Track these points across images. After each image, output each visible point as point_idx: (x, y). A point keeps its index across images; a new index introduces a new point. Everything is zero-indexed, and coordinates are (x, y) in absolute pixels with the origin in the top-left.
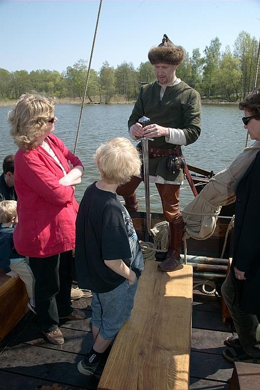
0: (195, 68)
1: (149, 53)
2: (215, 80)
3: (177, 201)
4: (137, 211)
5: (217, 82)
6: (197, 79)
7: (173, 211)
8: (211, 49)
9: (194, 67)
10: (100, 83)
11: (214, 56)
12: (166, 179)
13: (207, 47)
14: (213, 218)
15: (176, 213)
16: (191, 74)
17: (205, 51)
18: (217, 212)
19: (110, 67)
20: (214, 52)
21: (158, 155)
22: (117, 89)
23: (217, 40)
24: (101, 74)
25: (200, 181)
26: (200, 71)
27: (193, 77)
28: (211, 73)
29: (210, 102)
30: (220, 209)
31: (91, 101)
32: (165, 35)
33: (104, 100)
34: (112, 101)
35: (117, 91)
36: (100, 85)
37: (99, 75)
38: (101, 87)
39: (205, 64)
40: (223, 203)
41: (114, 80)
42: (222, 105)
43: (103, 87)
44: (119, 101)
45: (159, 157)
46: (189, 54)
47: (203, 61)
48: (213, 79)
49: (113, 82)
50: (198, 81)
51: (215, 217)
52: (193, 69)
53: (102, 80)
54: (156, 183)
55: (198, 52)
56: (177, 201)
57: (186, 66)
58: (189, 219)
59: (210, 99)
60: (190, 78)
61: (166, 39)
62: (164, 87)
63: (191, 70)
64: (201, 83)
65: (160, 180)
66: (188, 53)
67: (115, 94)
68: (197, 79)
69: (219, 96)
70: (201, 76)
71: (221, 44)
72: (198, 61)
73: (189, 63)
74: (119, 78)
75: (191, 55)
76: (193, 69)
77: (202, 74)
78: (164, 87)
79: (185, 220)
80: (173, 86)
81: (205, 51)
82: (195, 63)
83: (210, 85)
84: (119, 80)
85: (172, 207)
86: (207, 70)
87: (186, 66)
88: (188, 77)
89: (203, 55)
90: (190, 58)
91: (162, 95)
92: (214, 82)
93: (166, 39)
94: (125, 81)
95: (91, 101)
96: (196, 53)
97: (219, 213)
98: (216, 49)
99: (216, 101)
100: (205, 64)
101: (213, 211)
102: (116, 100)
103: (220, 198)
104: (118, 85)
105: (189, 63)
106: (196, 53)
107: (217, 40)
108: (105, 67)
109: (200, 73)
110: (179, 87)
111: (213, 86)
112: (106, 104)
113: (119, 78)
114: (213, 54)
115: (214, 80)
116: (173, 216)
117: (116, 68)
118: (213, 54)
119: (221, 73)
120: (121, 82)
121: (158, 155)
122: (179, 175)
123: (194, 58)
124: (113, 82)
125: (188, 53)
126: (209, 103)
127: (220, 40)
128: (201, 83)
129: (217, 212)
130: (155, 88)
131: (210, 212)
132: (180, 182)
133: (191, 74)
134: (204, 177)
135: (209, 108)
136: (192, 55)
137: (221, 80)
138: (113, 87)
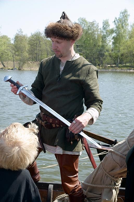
0: (105, 38)
1: (46, 30)
2: (124, 49)
3: (76, 172)
4: (39, 182)
5: (126, 51)
6: (107, 48)
7: (71, 182)
8: (120, 20)
9: (104, 37)
10: (13, 49)
11: (123, 27)
12: (65, 149)
13: (116, 18)
14: (114, 191)
15: (75, 185)
16: (100, 44)
17: (115, 22)
18: (117, 184)
19: (24, 34)
20: (123, 23)
21: (57, 126)
22: (31, 56)
23: (126, 11)
24: (15, 41)
25: (104, 150)
26: (110, 41)
27: (103, 46)
28: (120, 43)
29: (119, 70)
30: (120, 182)
31: (4, 66)
32: (63, 12)
33: (17, 66)
34: (25, 68)
35: (29, 58)
36: (13, 52)
37: (12, 42)
38: (15, 53)
39: (114, 35)
40: (123, 175)
41: (27, 47)
42: (130, 73)
43: (17, 53)
44: (32, 67)
45: (58, 127)
46: (99, 25)
47: (112, 31)
48: (121, 48)
49: (27, 49)
50: (107, 51)
51: (116, 190)
52: (103, 39)
53: (16, 47)
54: (56, 155)
55: (108, 23)
56: (76, 172)
57: (96, 36)
58: (90, 191)
59: (119, 67)
60: (100, 47)
61: (64, 16)
62: (64, 61)
63: (101, 40)
64: (110, 52)
65: (58, 151)
66: (98, 24)
67: (28, 60)
68: (107, 48)
69: (128, 64)
70: (110, 46)
71: (129, 15)
72: (108, 31)
73: (99, 33)
74: (32, 45)
75: (101, 26)
76: (103, 39)
77: (111, 43)
78: (64, 61)
79: (85, 192)
80: (73, 61)
81: (115, 22)
82: (105, 33)
83: (119, 54)
84: (33, 48)
85: (70, 179)
86: (116, 40)
87: (96, 36)
88: (98, 46)
89: (112, 26)
90: (100, 29)
91: (62, 68)
92: (122, 51)
93: (64, 16)
94: (38, 48)
95: (4, 66)
96: (106, 24)
97: (120, 185)
98: (124, 20)
99: (125, 70)
100: (114, 35)
101: (113, 183)
102: (29, 66)
103: (118, 171)
104: (31, 52)
105: (99, 33)
106: (106, 24)
107: (126, 11)
108: (18, 35)
109: (110, 42)
110: (79, 61)
111: (122, 55)
112: (19, 69)
113: (32, 45)
114: (122, 25)
115: (123, 50)
116: (73, 188)
117: (29, 35)
118: (122, 25)
119: (129, 43)
120: (35, 49)
121: (57, 126)
122: (77, 145)
123: (104, 28)
124: (27, 49)
125: (98, 24)
126: (119, 71)
127: (99, 24)
128: (110, 52)
129: (117, 184)
130: (55, 62)
131: (110, 185)
132: (79, 152)
133: (100, 44)
134: (108, 146)
135: (118, 76)
136: (102, 26)
137: (130, 49)
138: (26, 54)
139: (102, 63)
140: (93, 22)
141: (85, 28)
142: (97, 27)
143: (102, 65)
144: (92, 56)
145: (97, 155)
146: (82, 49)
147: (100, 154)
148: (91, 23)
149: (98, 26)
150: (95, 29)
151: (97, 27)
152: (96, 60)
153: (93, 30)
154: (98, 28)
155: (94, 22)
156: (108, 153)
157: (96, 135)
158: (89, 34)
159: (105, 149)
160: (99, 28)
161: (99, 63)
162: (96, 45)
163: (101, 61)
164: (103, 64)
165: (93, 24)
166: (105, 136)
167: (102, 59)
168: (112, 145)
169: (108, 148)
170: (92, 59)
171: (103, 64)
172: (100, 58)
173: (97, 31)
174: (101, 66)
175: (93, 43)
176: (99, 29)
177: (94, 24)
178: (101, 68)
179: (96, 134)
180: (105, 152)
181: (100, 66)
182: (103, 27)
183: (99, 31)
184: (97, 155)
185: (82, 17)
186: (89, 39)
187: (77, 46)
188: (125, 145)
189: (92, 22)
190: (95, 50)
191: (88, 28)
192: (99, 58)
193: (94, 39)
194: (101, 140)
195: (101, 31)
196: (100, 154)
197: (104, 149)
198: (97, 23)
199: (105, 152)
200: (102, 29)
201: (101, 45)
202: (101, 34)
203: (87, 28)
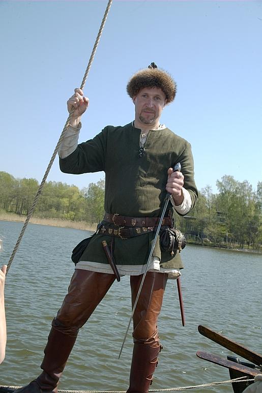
16: (253, 213)
25: (244, 374)
27: (256, 218)
63: (253, 208)
66: (251, 186)
73: (252, 198)
87: (247, 203)
93: (154, 66)
105: (252, 198)
134: (253, 367)
136: (256, 190)
139: (253, 241)
140: (244, 183)
141: (231, 190)
142: (250, 190)
143: (252, 244)
144: (238, 228)
145: (228, 381)
146: (224, 217)
147: (235, 380)
148: (241, 184)
149: (251, 190)
150: (246, 192)
151: (250, 190)
152: (245, 235)
153: (244, 193)
154: (250, 191)
155: (245, 183)
156: (253, 380)
157: (230, 342)
158: (237, 198)
159: (245, 372)
160: (252, 191)
161: (248, 240)
162: (246, 215)
163: (252, 238)
164: (254, 243)
165: (243, 185)
166: (238, 340)
167: (253, 235)
168: (259, 366)
169: (252, 371)
170: (239, 234)
171: (254, 243)
172: (250, 234)
173: (249, 196)
174: (251, 246)
175: (241, 212)
176: (252, 194)
177: (245, 186)
178: (250, 247)
179: (238, 344)
180: (246, 377)
181: (250, 244)
182: (258, 191)
183: (252, 196)
184: (228, 381)
185: (228, 175)
186: (235, 205)
187: (218, 213)
188: (120, 339)
189: (242, 182)
190: (243, 222)
191: (236, 191)
192: (249, 233)
193: (243, 207)
194: (239, 352)
195: (254, 197)
196: (235, 380)
197: (242, 371)
198: (249, 185)
199: (246, 377)
200: (256, 193)
201: (253, 216)
202: (255, 200)
203: (234, 190)
